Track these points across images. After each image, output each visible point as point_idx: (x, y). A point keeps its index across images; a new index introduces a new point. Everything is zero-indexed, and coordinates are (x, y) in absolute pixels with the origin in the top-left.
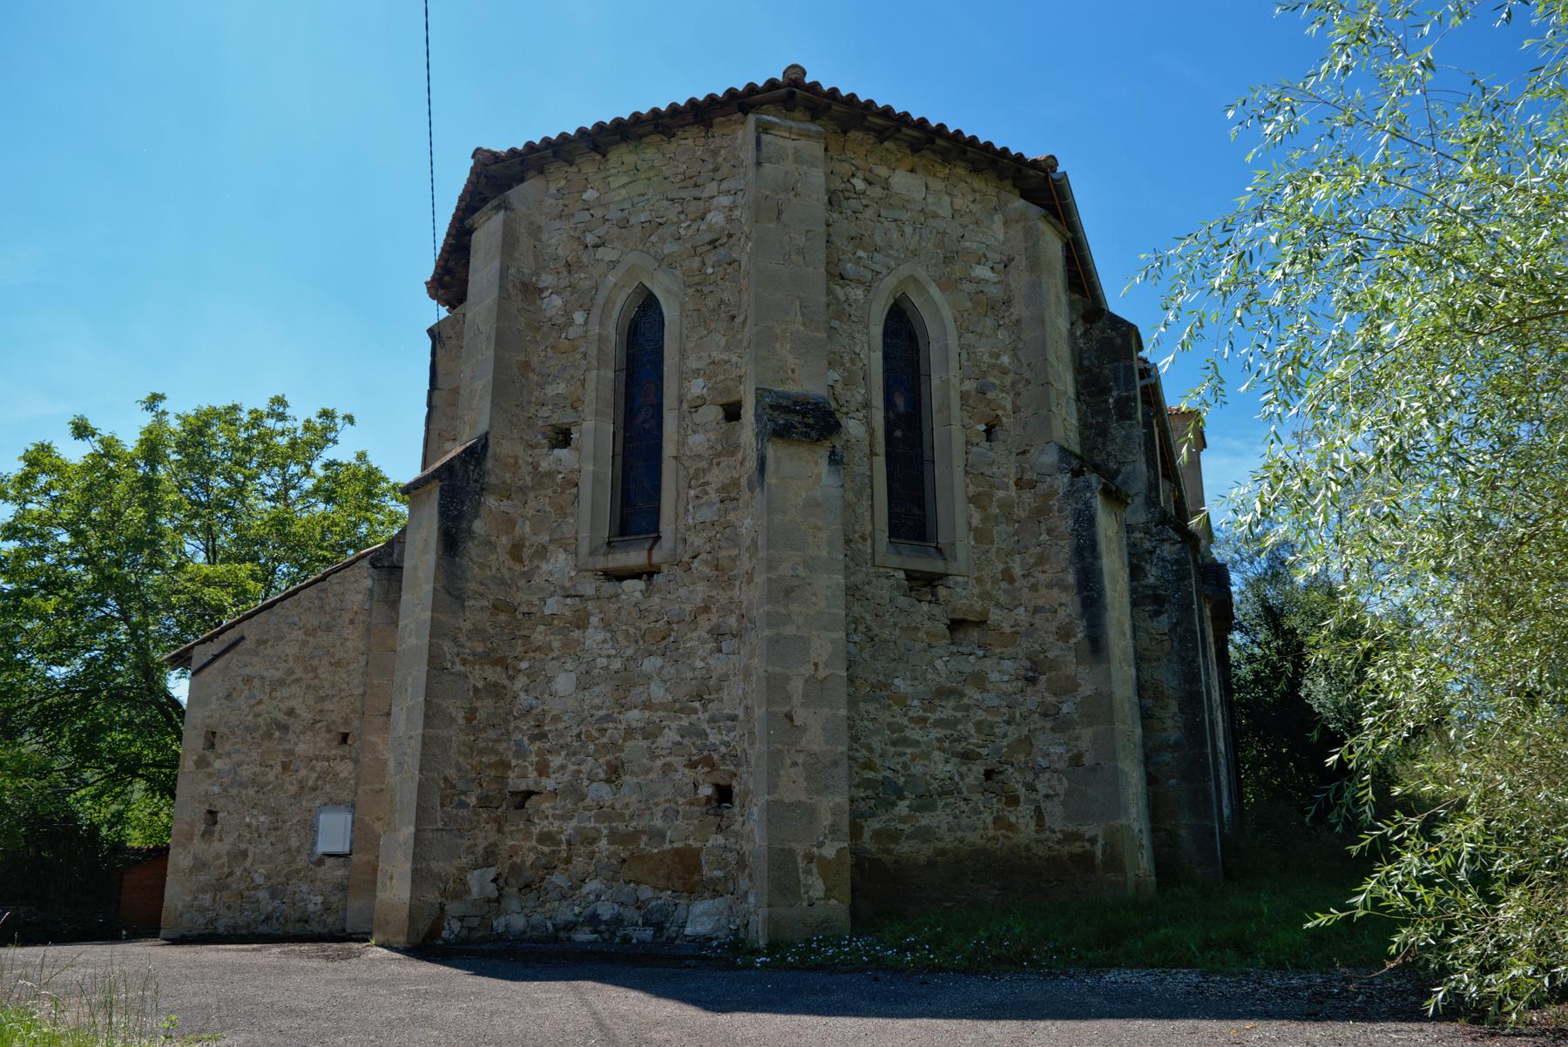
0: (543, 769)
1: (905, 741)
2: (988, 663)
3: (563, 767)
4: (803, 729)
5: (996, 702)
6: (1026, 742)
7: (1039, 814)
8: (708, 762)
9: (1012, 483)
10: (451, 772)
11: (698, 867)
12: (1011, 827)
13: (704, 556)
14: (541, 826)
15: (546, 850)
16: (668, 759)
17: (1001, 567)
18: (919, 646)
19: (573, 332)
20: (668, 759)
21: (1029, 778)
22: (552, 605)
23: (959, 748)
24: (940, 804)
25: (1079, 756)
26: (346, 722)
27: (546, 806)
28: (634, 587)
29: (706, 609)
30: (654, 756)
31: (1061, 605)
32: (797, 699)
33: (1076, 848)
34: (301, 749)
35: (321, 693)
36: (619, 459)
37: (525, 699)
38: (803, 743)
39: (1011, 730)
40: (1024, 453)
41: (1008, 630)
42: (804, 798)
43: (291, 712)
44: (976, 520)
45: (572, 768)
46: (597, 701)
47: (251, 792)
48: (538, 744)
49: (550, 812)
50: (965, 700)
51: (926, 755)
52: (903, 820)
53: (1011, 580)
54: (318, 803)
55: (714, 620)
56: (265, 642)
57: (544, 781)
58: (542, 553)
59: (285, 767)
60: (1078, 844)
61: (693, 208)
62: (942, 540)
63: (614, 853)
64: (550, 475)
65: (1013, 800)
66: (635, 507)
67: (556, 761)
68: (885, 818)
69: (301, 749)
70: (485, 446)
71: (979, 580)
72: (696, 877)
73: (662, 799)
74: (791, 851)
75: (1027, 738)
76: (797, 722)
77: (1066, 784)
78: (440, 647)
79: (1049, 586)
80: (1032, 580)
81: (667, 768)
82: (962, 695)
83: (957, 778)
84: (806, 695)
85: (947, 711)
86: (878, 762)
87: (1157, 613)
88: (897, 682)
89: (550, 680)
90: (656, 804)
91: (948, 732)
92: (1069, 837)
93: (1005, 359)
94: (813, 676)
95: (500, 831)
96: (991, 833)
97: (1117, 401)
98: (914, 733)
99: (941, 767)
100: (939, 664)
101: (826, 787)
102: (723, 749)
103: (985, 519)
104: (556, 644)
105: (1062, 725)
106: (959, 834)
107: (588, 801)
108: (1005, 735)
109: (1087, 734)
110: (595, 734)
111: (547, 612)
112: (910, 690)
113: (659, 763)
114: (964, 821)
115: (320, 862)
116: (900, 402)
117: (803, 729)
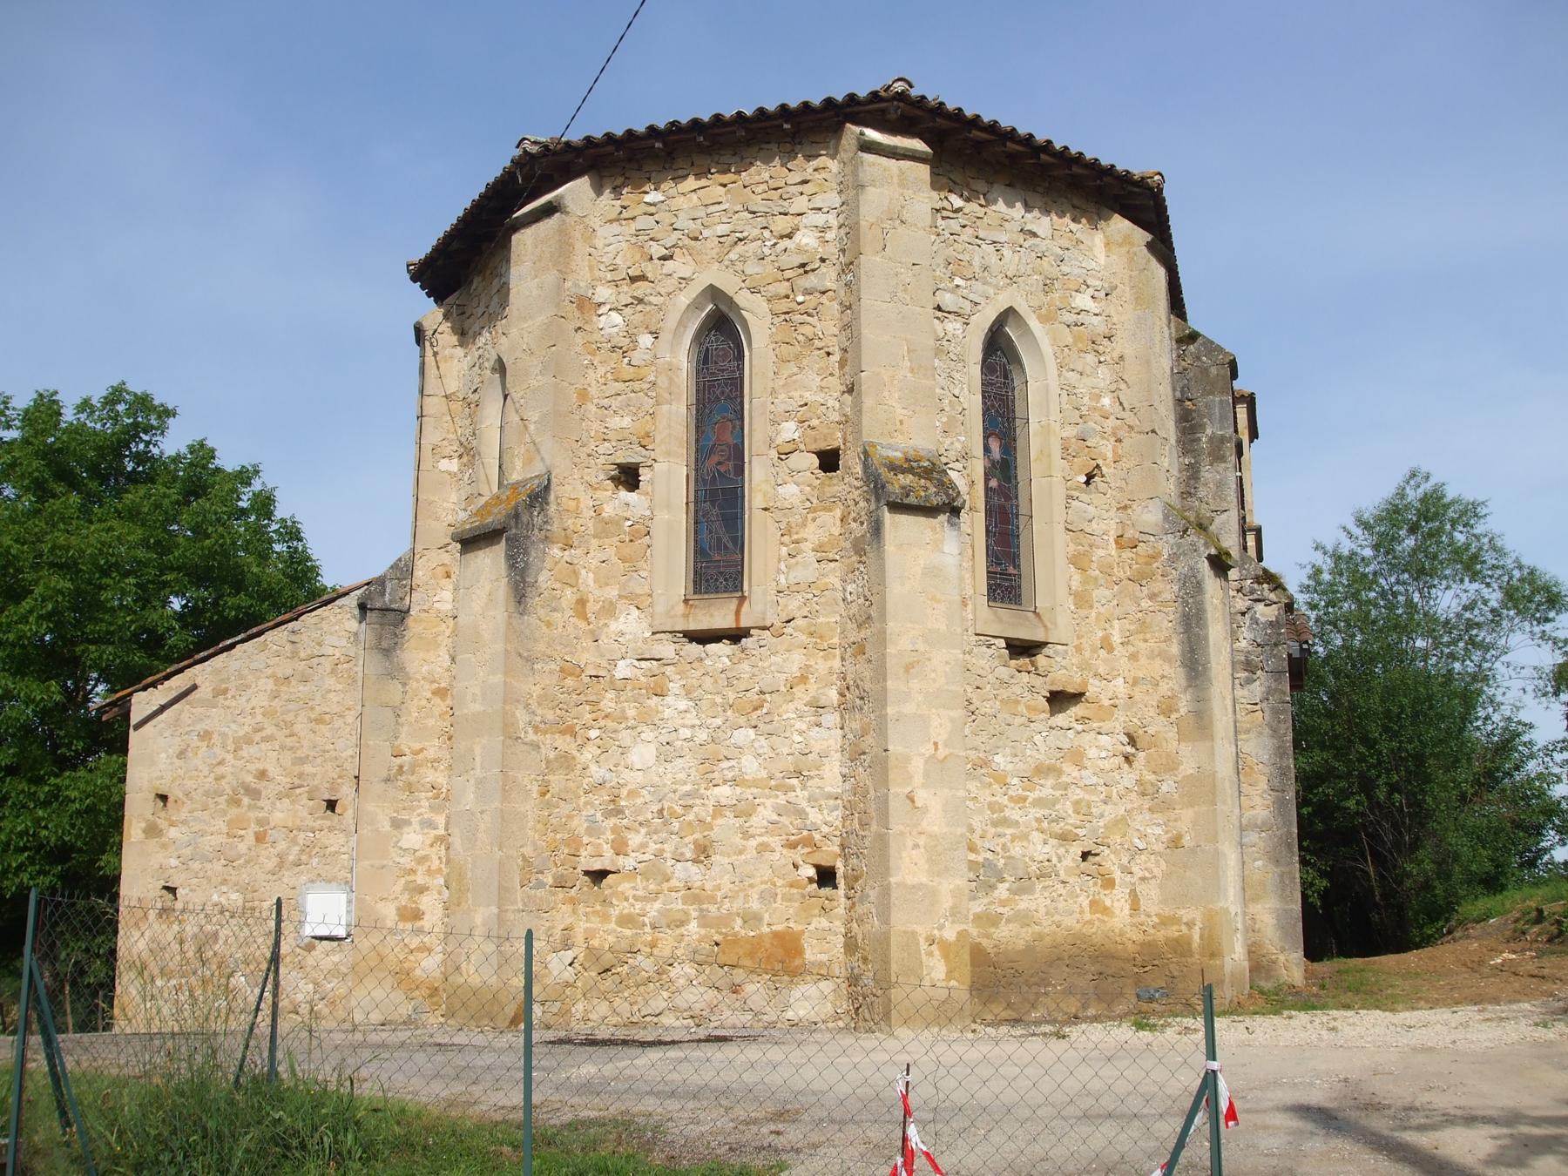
0: (620, 849)
1: (1005, 822)
2: (1087, 737)
3: (643, 845)
4: (924, 810)
5: (1094, 780)
6: (1121, 823)
7: (1134, 899)
8: (809, 842)
9: (1112, 540)
10: (528, 851)
11: (800, 952)
12: (1106, 911)
13: (799, 622)
14: (620, 908)
15: (628, 932)
16: (765, 839)
17: (1100, 634)
18: (1018, 720)
19: (637, 357)
20: (765, 839)
21: (1125, 861)
22: (623, 670)
23: (1057, 828)
24: (1039, 886)
25: (1179, 837)
26: (334, 787)
27: (625, 887)
28: (722, 649)
29: (803, 679)
30: (746, 835)
31: (1163, 677)
32: (918, 780)
33: (1173, 931)
34: (278, 817)
35: (299, 754)
36: (692, 506)
37: (597, 772)
38: (924, 824)
39: (1108, 808)
40: (1125, 507)
41: (1106, 703)
42: (924, 880)
43: (262, 775)
44: (1075, 584)
45: (653, 847)
46: (682, 776)
47: (218, 866)
48: (613, 821)
49: (630, 893)
50: (1064, 779)
51: (1025, 837)
52: (1003, 903)
53: (1111, 650)
54: (303, 878)
55: (812, 692)
56: (225, 691)
57: (621, 860)
58: (609, 610)
59: (260, 838)
60: (1175, 928)
61: (782, 225)
62: (1041, 603)
63: (706, 936)
64: (615, 522)
65: (1109, 883)
66: (718, 557)
67: (635, 839)
68: (986, 901)
69: (278, 817)
70: (547, 488)
71: (1078, 649)
72: (797, 962)
73: (758, 880)
74: (914, 934)
75: (1123, 818)
76: (918, 804)
77: (1163, 865)
78: (513, 715)
79: (1152, 657)
80: (1131, 649)
81: (763, 848)
82: (1060, 772)
83: (1055, 860)
84: (926, 775)
85: (1046, 789)
86: (979, 842)
87: (1249, 681)
88: (997, 758)
89: (624, 750)
90: (752, 886)
91: (1046, 812)
92: (1165, 921)
93: (1106, 401)
94: (933, 756)
95: (574, 912)
96: (1087, 916)
97: (1211, 439)
98: (1014, 814)
99: (1039, 848)
100: (1038, 738)
101: (947, 869)
102: (825, 829)
103: (1084, 582)
104: (631, 713)
105: (1162, 806)
106: (1057, 918)
107: (674, 883)
108: (1102, 816)
109: (1187, 815)
110: (679, 810)
111: (619, 675)
112: (1010, 767)
113: (753, 843)
114: (1061, 905)
115: (310, 948)
116: (995, 446)
117: (924, 810)
